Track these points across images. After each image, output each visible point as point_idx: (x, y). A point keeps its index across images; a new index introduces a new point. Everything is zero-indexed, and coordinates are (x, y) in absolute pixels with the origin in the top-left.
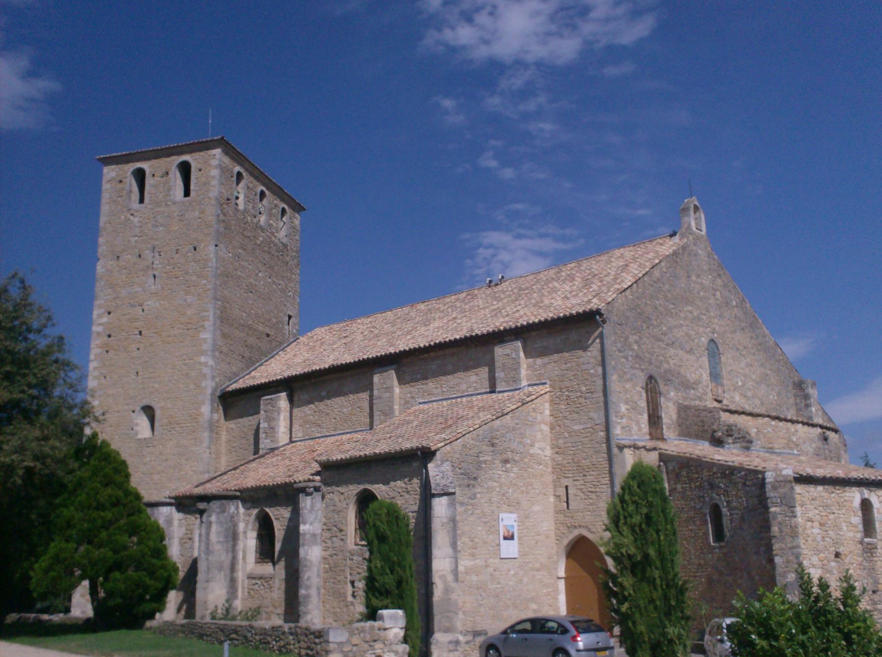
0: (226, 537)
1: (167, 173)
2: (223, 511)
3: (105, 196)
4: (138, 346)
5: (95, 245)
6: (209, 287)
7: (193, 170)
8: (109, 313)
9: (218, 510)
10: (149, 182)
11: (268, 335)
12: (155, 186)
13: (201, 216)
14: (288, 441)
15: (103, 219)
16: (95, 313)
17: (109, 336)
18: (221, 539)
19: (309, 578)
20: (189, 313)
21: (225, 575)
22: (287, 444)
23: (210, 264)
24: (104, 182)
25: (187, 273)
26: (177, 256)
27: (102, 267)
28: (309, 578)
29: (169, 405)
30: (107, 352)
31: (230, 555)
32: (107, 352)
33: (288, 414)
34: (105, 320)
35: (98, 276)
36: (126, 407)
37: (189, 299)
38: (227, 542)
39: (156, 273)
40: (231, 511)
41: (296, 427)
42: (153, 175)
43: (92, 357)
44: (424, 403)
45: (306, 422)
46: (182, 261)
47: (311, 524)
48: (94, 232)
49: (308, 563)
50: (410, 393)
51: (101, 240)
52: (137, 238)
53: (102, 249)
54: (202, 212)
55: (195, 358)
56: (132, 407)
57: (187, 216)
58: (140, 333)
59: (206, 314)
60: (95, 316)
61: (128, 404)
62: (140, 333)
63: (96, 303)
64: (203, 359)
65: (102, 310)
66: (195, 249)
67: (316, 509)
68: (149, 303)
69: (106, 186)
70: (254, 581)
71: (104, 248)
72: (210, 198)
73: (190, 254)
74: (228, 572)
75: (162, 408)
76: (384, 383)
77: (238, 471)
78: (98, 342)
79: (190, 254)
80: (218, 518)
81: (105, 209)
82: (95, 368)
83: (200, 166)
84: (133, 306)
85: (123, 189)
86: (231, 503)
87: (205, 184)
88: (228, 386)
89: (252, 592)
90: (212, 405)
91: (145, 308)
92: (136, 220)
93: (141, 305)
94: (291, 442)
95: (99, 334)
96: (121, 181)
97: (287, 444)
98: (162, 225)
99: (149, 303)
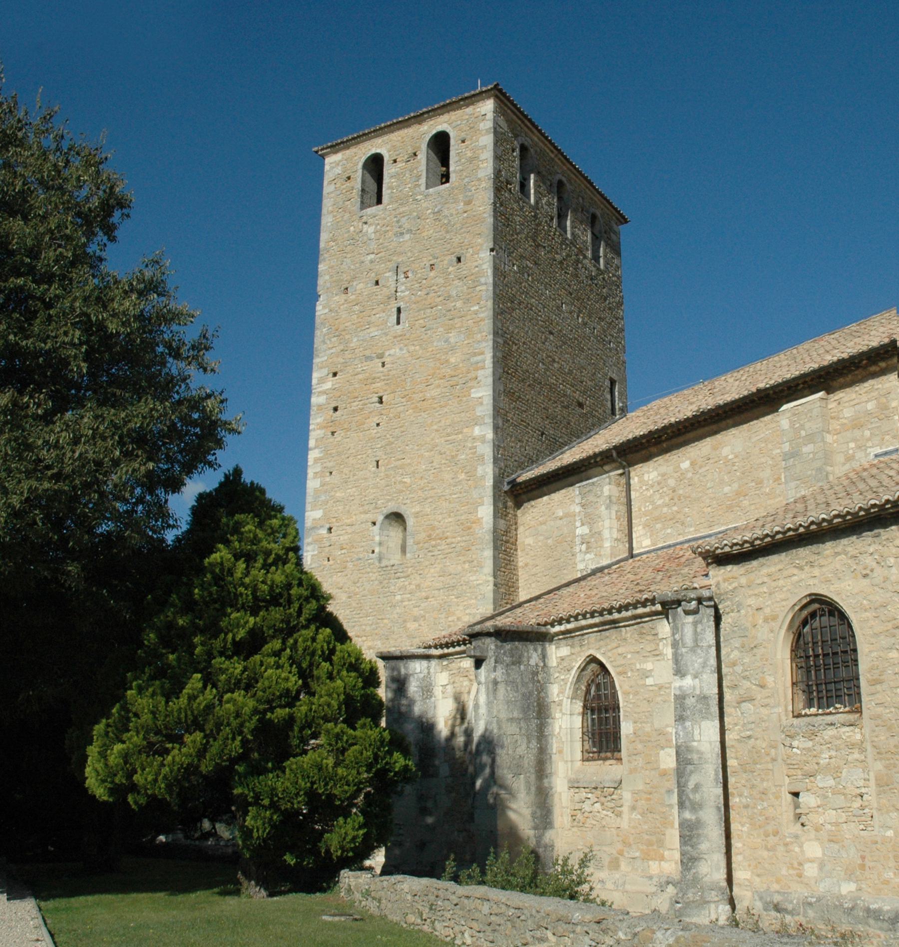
0: (525, 710)
1: (415, 154)
2: (518, 662)
3: (328, 204)
4: (376, 420)
5: (314, 275)
6: (482, 315)
7: (452, 142)
8: (335, 374)
9: (507, 659)
10: (388, 171)
11: (581, 405)
12: (396, 176)
13: (468, 208)
14: (626, 555)
15: (324, 236)
16: (316, 376)
17: (336, 409)
18: (516, 714)
19: (697, 787)
20: (453, 360)
21: (528, 782)
22: (626, 559)
23: (483, 280)
24: (325, 183)
25: (448, 298)
26: (432, 274)
27: (324, 307)
28: (697, 787)
29: (428, 510)
30: (333, 433)
31: (534, 744)
32: (333, 433)
33: (624, 509)
34: (328, 385)
35: (318, 321)
36: (364, 517)
37: (453, 337)
38: (526, 719)
39: (402, 305)
40: (532, 662)
41: (638, 531)
42: (395, 161)
43: (312, 443)
44: (886, 453)
45: (657, 519)
46: (441, 281)
47: (695, 677)
48: (312, 254)
49: (695, 756)
50: (854, 440)
51: (322, 267)
52: (372, 256)
53: (324, 280)
54: (468, 203)
55: (465, 430)
56: (370, 517)
57: (446, 212)
58: (381, 401)
59: (479, 358)
60: (314, 381)
61: (366, 513)
62: (381, 401)
63: (316, 361)
64: (477, 431)
65: (325, 371)
66: (459, 260)
67: (704, 644)
68: (392, 352)
69: (328, 188)
70: (583, 794)
71: (327, 277)
72: (479, 180)
73: (451, 269)
74: (533, 778)
75: (417, 515)
76: (802, 427)
77: (542, 600)
78: (319, 420)
79: (451, 269)
80: (508, 674)
81: (327, 220)
82: (316, 460)
83: (463, 135)
84: (368, 358)
85: (353, 188)
86: (531, 647)
87: (471, 160)
88: (519, 476)
89: (579, 816)
90: (495, 505)
91: (387, 360)
92: (371, 229)
93: (380, 356)
94: (632, 556)
95: (320, 406)
96: (349, 178)
97: (626, 559)
98: (409, 231)
99: (392, 352)
